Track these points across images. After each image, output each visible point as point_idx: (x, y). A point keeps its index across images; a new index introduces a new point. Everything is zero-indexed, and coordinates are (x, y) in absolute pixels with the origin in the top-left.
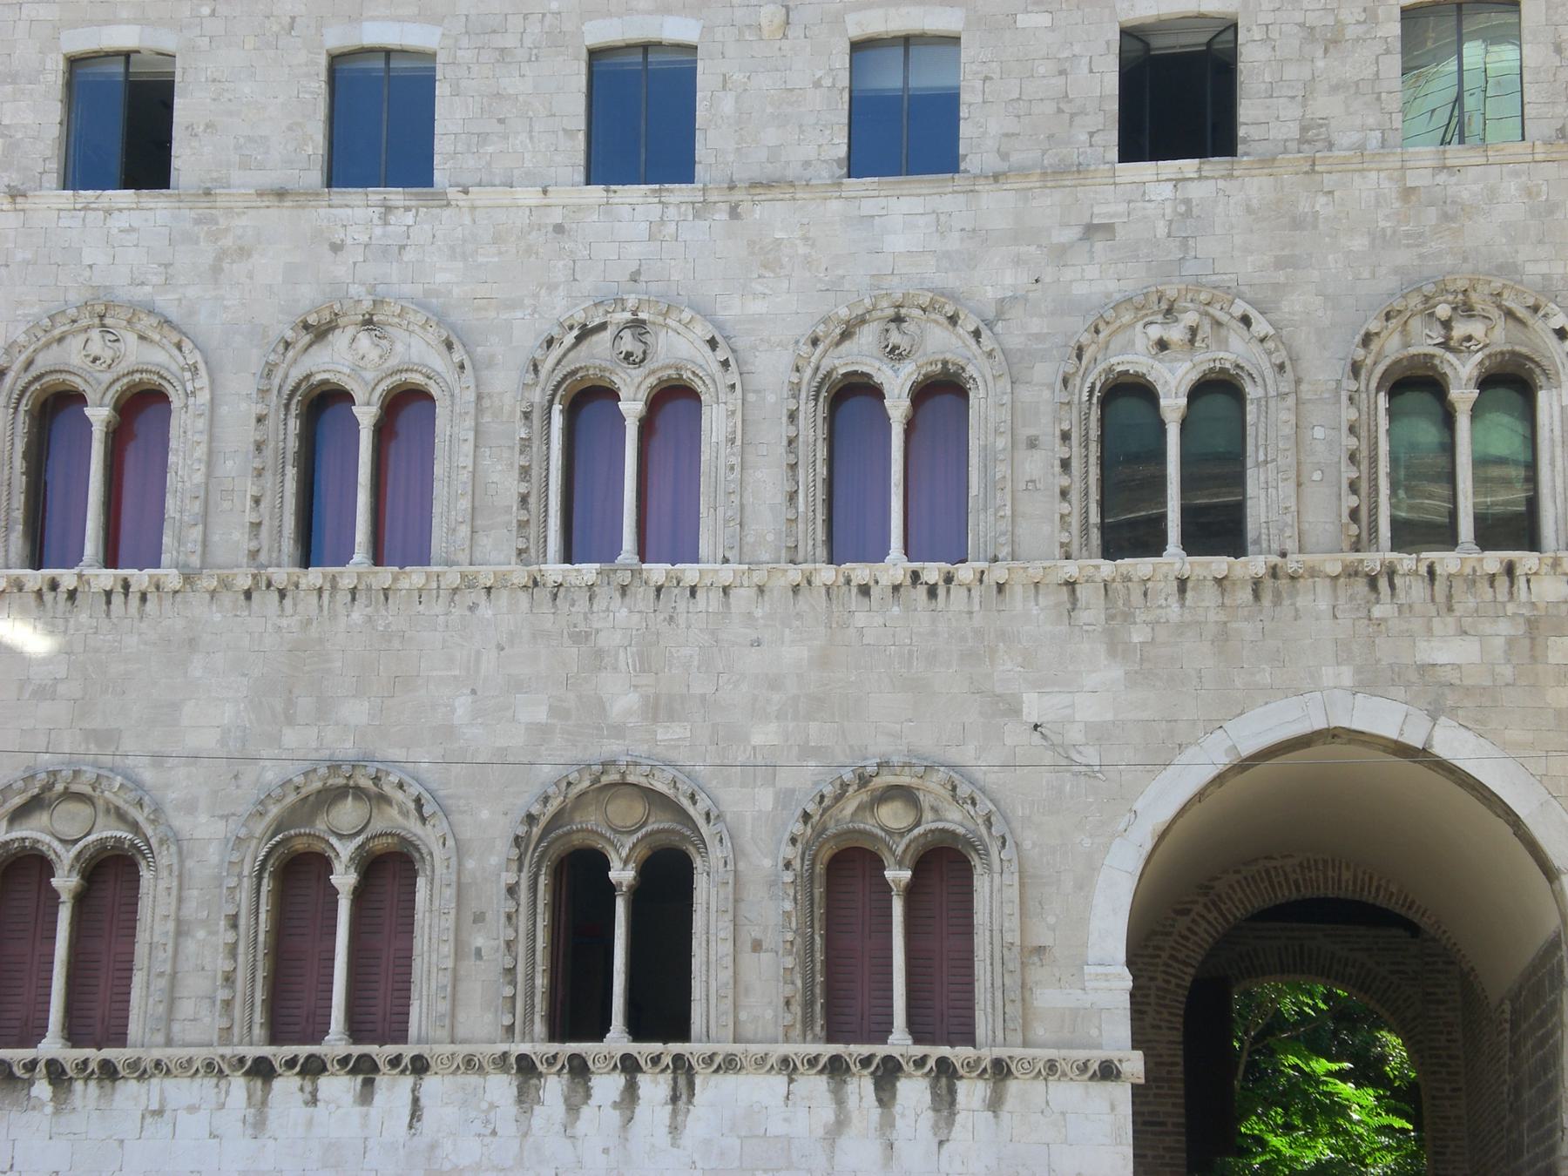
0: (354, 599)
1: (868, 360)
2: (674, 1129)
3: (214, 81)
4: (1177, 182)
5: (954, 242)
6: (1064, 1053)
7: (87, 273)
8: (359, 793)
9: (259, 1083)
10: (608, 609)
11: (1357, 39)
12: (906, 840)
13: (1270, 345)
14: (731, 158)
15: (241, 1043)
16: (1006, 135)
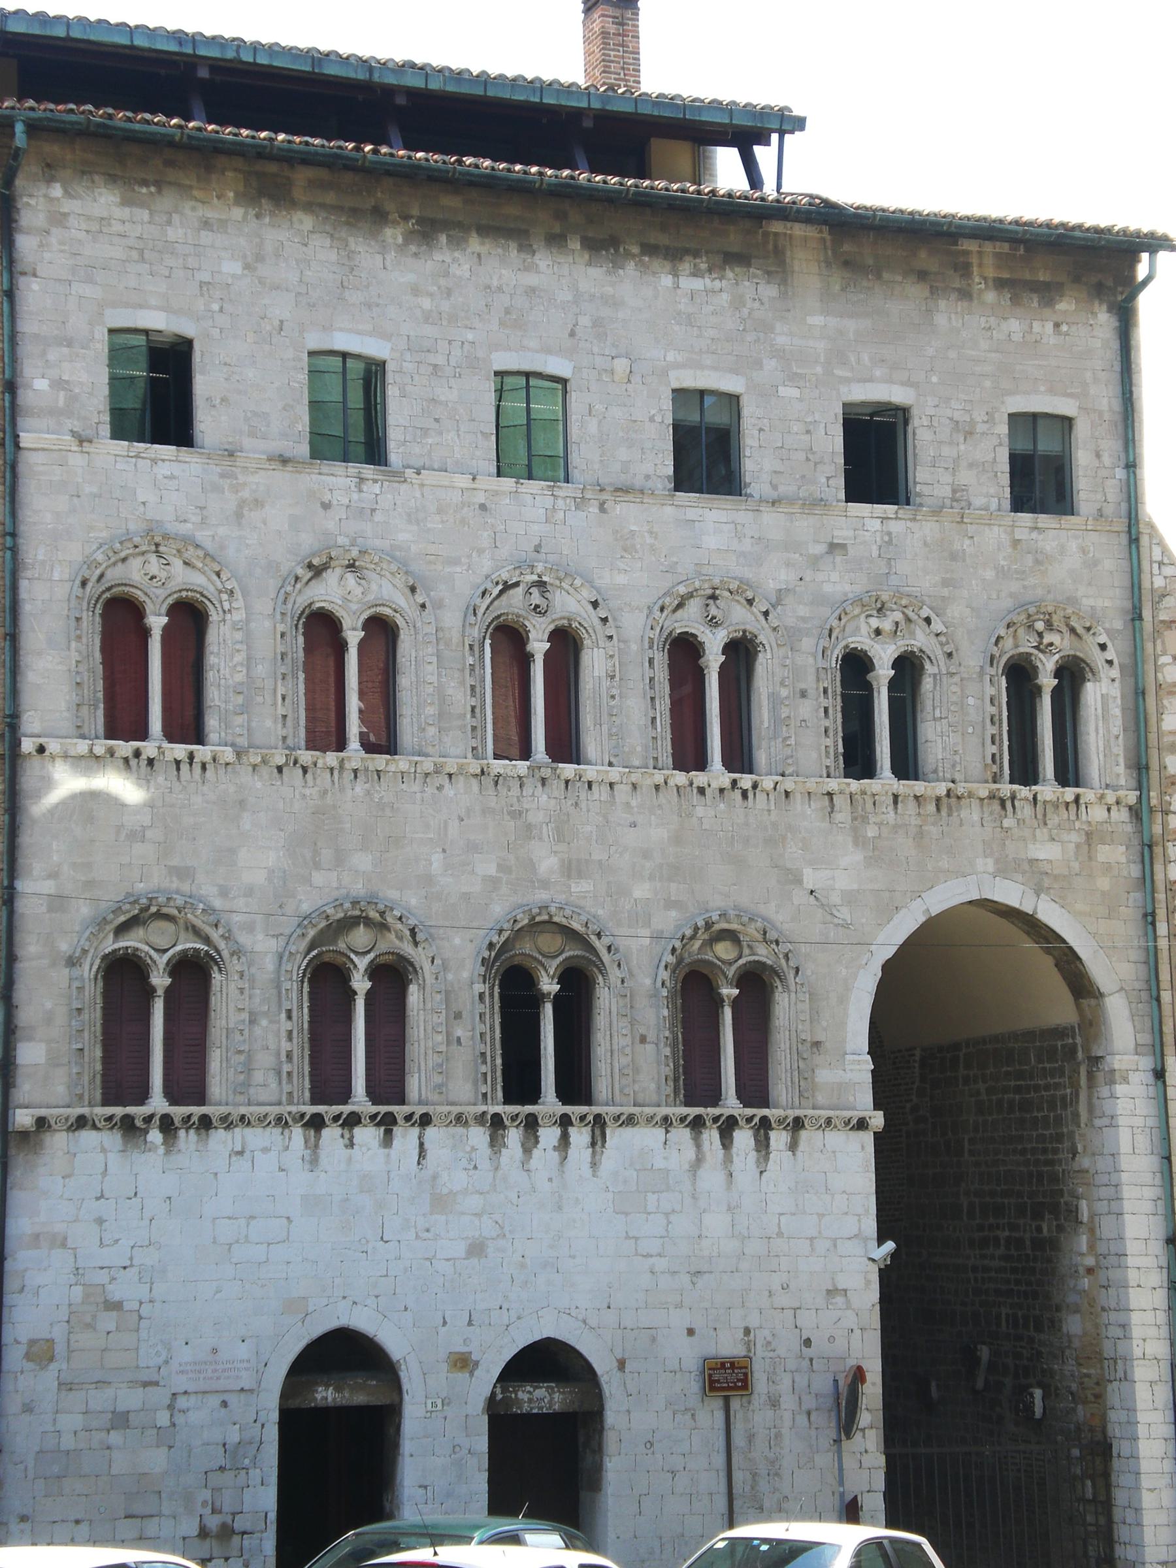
0: (356, 777)
1: (696, 625)
2: (594, 1165)
3: (225, 364)
4: (884, 519)
5: (747, 545)
6: (838, 1113)
7: (142, 509)
8: (368, 922)
9: (312, 1132)
10: (533, 795)
11: (983, 434)
12: (734, 968)
13: (943, 639)
14: (596, 466)
15: (298, 1104)
16: (775, 472)
